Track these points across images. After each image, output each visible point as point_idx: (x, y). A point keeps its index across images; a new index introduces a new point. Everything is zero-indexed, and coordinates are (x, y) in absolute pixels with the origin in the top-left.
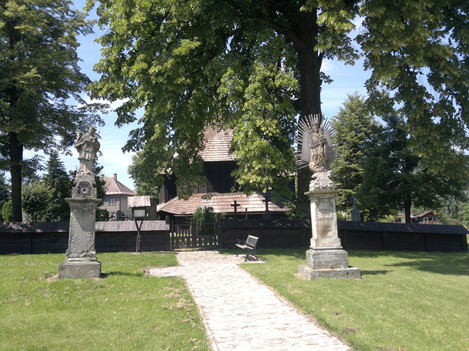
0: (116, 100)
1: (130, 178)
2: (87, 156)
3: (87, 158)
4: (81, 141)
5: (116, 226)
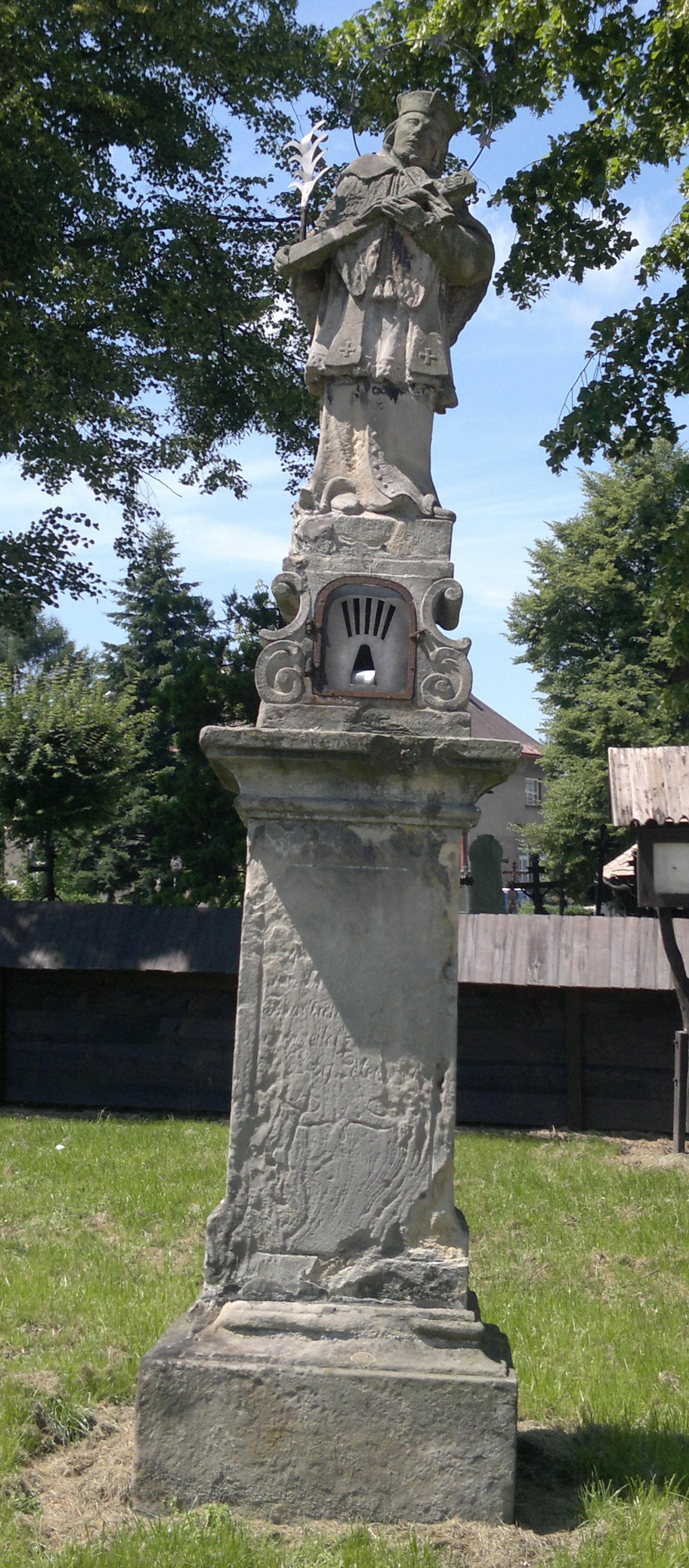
0: (510, 115)
1: (519, 661)
2: (384, 350)
3: (381, 368)
4: (334, 220)
5: (522, 949)
